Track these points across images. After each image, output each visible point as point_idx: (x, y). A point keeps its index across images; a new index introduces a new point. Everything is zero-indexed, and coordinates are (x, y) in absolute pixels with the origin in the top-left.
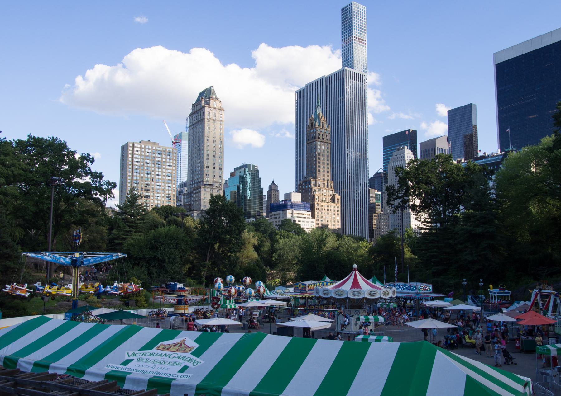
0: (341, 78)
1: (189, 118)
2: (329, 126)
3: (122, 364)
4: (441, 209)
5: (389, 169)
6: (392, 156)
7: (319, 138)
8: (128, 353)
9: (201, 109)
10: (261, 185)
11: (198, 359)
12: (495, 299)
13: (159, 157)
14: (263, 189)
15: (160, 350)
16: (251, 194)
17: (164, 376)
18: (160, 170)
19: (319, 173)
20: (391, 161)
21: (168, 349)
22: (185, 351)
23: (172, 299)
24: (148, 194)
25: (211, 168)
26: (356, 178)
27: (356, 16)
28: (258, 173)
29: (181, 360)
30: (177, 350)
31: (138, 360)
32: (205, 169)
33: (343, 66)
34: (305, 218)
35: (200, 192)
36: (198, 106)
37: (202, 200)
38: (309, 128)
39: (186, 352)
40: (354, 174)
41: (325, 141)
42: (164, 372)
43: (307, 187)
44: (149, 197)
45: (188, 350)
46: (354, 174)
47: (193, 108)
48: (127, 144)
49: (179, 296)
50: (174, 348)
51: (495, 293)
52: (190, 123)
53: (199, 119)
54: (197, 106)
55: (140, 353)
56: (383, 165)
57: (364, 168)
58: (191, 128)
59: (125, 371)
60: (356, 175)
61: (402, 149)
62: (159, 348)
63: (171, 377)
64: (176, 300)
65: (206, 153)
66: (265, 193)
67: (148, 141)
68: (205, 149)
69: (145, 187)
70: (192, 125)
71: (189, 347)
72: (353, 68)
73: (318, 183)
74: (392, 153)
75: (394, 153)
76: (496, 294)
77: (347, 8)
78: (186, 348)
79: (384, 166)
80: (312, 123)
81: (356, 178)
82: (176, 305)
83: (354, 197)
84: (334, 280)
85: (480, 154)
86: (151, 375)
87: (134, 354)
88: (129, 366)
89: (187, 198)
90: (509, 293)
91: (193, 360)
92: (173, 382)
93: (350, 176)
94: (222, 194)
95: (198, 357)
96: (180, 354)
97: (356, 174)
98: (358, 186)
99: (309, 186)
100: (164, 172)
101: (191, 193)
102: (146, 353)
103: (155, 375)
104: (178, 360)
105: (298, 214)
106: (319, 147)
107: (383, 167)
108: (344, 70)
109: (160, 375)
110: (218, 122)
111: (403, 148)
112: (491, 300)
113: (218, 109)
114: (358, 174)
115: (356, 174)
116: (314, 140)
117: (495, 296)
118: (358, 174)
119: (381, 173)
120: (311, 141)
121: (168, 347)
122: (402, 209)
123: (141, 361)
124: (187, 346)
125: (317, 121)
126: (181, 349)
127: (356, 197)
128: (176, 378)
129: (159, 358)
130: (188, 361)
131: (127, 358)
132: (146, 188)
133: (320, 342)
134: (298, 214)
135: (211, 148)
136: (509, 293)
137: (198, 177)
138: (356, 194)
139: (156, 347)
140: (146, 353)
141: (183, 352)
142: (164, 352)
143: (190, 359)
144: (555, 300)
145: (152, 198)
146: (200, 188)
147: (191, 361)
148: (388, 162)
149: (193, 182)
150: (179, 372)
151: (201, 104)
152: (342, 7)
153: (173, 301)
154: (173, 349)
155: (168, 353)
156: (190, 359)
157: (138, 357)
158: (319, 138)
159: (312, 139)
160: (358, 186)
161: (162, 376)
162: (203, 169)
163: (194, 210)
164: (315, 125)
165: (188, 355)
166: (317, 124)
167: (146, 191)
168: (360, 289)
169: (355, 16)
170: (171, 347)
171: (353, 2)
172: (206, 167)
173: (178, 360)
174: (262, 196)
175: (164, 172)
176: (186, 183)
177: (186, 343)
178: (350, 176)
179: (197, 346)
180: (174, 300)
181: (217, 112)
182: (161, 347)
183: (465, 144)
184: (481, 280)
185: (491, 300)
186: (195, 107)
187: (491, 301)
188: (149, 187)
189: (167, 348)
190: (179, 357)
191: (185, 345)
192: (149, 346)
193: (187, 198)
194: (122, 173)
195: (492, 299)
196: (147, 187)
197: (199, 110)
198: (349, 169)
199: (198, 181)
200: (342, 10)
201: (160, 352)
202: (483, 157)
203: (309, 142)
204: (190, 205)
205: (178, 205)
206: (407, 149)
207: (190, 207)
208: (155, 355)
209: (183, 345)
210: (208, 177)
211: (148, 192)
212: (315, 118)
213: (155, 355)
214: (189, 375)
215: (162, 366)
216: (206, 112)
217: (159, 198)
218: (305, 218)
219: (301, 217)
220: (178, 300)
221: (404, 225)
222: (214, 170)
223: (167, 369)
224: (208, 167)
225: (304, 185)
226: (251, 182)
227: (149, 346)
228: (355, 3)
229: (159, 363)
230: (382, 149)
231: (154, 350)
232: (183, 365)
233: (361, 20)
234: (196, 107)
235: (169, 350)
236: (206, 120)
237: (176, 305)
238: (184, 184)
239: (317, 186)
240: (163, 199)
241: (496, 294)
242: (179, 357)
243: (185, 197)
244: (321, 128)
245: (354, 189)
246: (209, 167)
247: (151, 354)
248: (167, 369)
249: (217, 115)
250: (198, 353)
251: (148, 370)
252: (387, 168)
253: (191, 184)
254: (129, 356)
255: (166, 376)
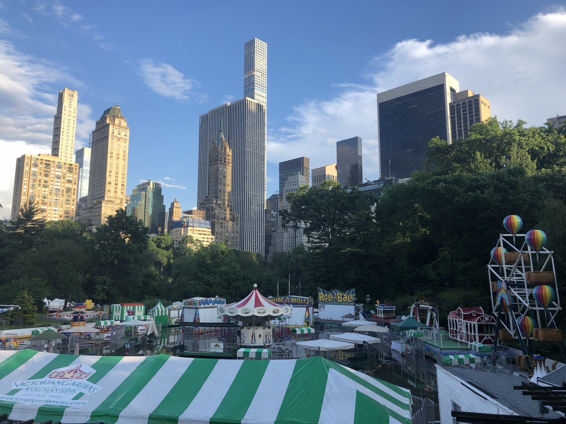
0: (243, 107)
1: (93, 134)
2: (231, 150)
3: (8, 394)
4: (329, 230)
5: (284, 191)
6: (287, 180)
7: (221, 161)
8: (55, 151)
9: (105, 126)
10: (163, 203)
11: (95, 386)
12: (381, 314)
13: (59, 171)
14: (165, 206)
15: (52, 378)
16: (152, 211)
17: (57, 404)
18: (59, 184)
19: (220, 193)
20: (286, 185)
21: (61, 376)
22: (80, 377)
23: (67, 316)
24: (45, 207)
25: (113, 184)
26: (254, 199)
27: (258, 51)
28: (161, 191)
29: (76, 387)
30: (72, 377)
31: (27, 389)
32: (107, 185)
33: (245, 97)
34: (205, 234)
35: (101, 207)
36: (102, 123)
37: (102, 215)
38: (212, 151)
39: (81, 378)
40: (252, 195)
41: (222, 163)
42: (56, 399)
43: (208, 205)
44: (46, 211)
45: (83, 376)
46: (252, 195)
47: (98, 125)
48: (23, 157)
49: (76, 313)
50: (69, 374)
51: (381, 308)
52: (93, 139)
53: (103, 137)
54: (101, 123)
55: (30, 382)
56: (278, 188)
57: (256, 189)
58: (94, 144)
59: (11, 401)
60: (254, 196)
61: (296, 174)
62: (51, 376)
63: (64, 405)
64: (72, 317)
65: (108, 169)
66: (167, 210)
67: (48, 154)
68: (108, 166)
69: (42, 200)
70: (95, 142)
71: (85, 373)
72: (254, 99)
73: (219, 202)
74: (287, 177)
75: (289, 178)
76: (382, 309)
77: (250, 43)
78: (82, 374)
79: (280, 189)
80: (215, 147)
81: (254, 199)
82: (72, 321)
83: (252, 216)
84: (18, 50)
85: (364, 181)
86: (41, 404)
87: (23, 384)
88: (16, 396)
89: (86, 213)
90: (394, 308)
91: (89, 386)
92: (67, 409)
93: (248, 197)
94: (124, 209)
95: (95, 383)
96: (74, 380)
97: (254, 195)
98: (256, 206)
99: (211, 205)
100: (63, 186)
101: (91, 208)
102: (36, 382)
103: (46, 403)
104: (71, 387)
105: (199, 231)
106: (221, 169)
107: (278, 190)
108: (246, 100)
109: (51, 404)
110: (122, 140)
111: (298, 174)
112: (378, 315)
113: (123, 128)
114: (256, 196)
115: (254, 195)
116: (216, 163)
117: (381, 310)
118: (256, 196)
119: (277, 195)
120: (213, 164)
121: (61, 374)
122: (295, 229)
123: (30, 390)
124: (83, 372)
125: (220, 145)
126: (76, 375)
127: (254, 216)
128: (70, 405)
129: (51, 386)
130: (84, 388)
131: (14, 387)
132: (43, 202)
133: (220, 361)
134: (199, 231)
135: (114, 165)
136: (394, 308)
137: (99, 192)
138: (254, 213)
139: (49, 374)
140: (36, 382)
141: (78, 378)
142: (56, 380)
143: (86, 386)
144: (432, 315)
145: (50, 211)
146: (101, 203)
147: (86, 388)
148: (284, 185)
149: (94, 198)
150: (73, 399)
151: (106, 121)
152: (246, 43)
153: (68, 318)
154: (67, 375)
155: (61, 380)
156: (86, 386)
157: (27, 386)
158: (221, 161)
159: (214, 161)
160: (256, 206)
161: (53, 404)
162: (105, 185)
163: (93, 225)
164: (217, 149)
165: (84, 381)
166: (220, 148)
167: (43, 205)
168: (262, 307)
169: (257, 51)
170: (65, 374)
171: (256, 38)
172: (108, 183)
173: (71, 387)
174: (164, 213)
175: (63, 186)
176: (86, 198)
177: (81, 369)
178: (248, 197)
179: (94, 371)
180: (70, 317)
181: (121, 131)
182: (54, 375)
183: (351, 172)
184: (368, 296)
185: (378, 315)
186: (99, 124)
187: (378, 316)
188: (46, 200)
189: (60, 375)
190: (74, 384)
191: (80, 371)
192: (41, 374)
193: (86, 213)
194: (17, 186)
195: (379, 314)
196: (44, 200)
197: (103, 128)
198: (248, 191)
199: (98, 196)
200: (245, 44)
201: (52, 380)
202: (367, 184)
203: (212, 164)
204: (90, 220)
205: (76, 219)
206: (301, 174)
207: (89, 222)
208: (46, 383)
209: (78, 372)
210: (110, 193)
211: (45, 205)
212: (218, 142)
213: (46, 383)
214: (84, 402)
215: (54, 394)
216: (110, 129)
217: (57, 212)
218: (205, 234)
219: (201, 234)
220: (74, 317)
221: (296, 242)
222: (116, 186)
223: (59, 397)
224: (110, 183)
225: (205, 204)
226: (153, 199)
227: (41, 374)
228: (258, 39)
229: (51, 391)
230: (279, 173)
231: (46, 378)
232: (77, 393)
233: (260, 54)
234: (100, 124)
235: (63, 377)
236: (110, 137)
237: (72, 321)
238: (84, 199)
239: (218, 205)
240: (61, 213)
241: (382, 309)
242: (74, 384)
243: (85, 212)
244: (223, 151)
245: (252, 209)
246: (111, 183)
247: (41, 383)
248: (59, 397)
249: (122, 133)
250: (94, 379)
251: (38, 399)
252: (282, 191)
253: (91, 200)
254: (17, 386)
255: (59, 404)
